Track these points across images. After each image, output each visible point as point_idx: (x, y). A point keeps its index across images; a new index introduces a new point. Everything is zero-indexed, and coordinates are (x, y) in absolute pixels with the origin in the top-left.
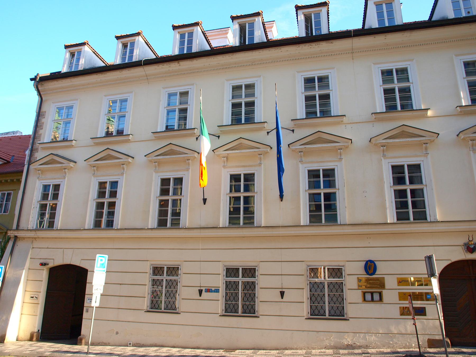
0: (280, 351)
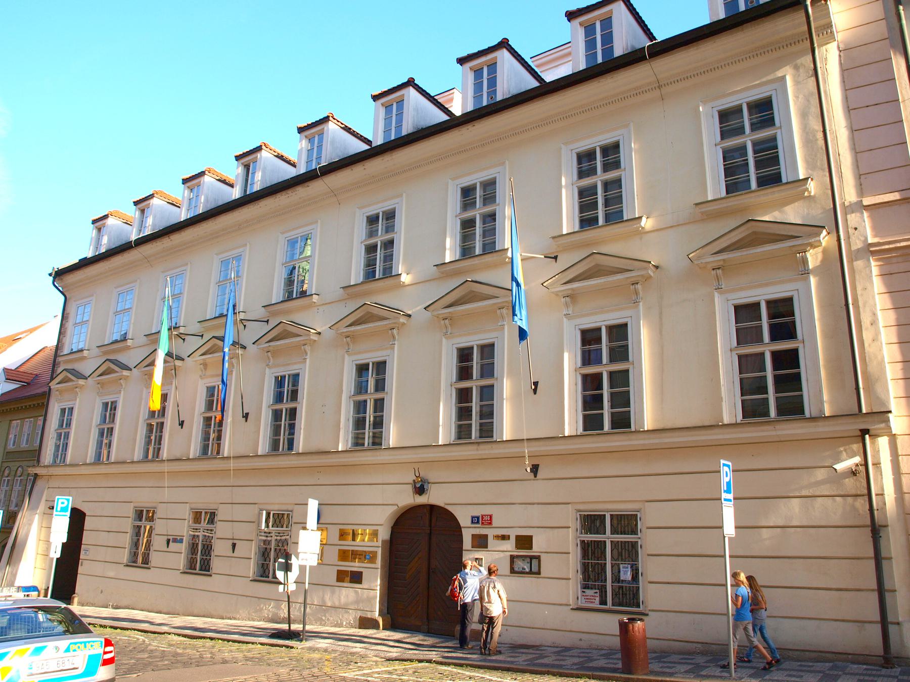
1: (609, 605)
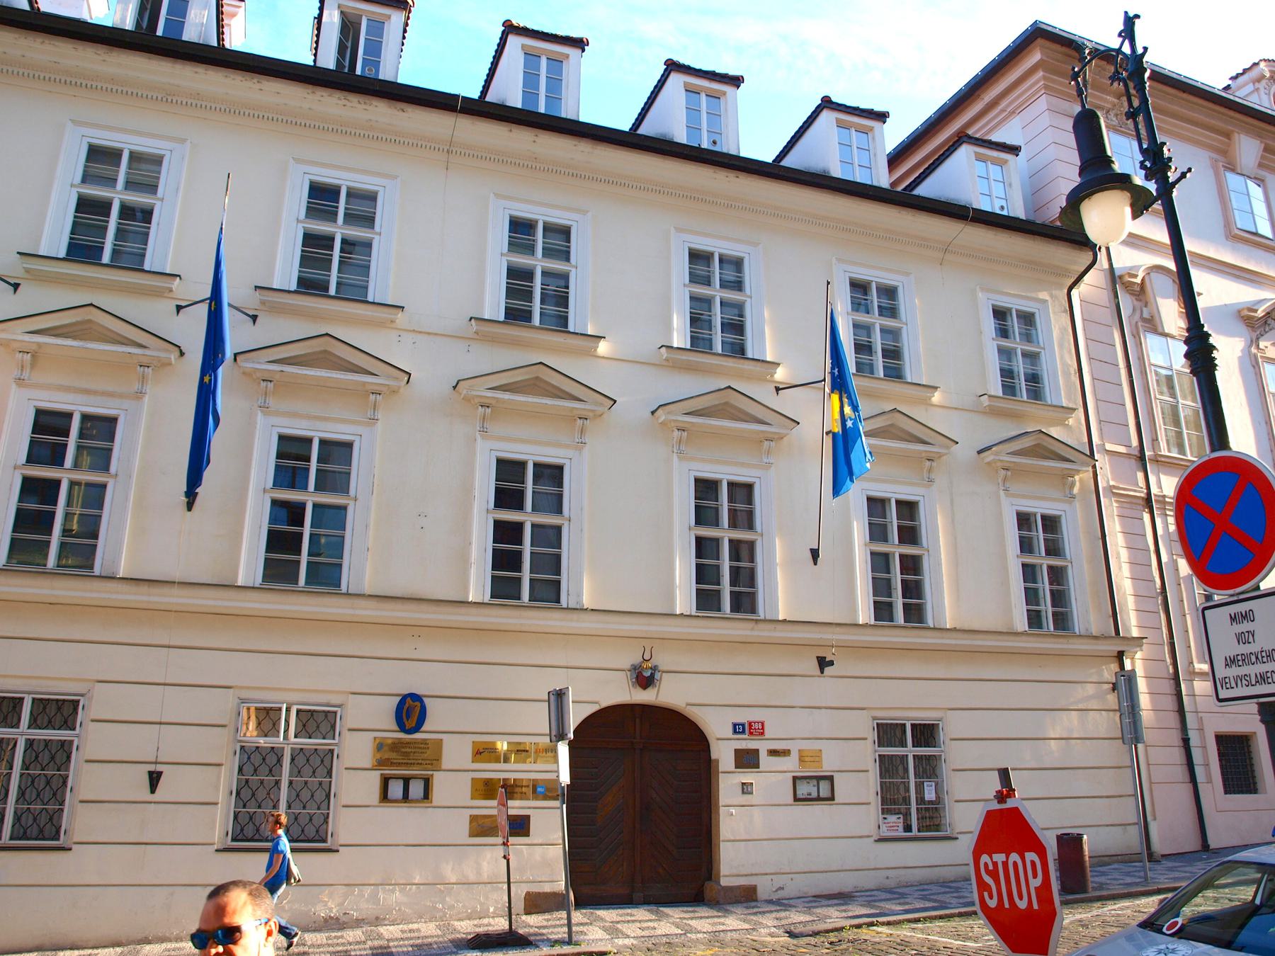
0: (125, 948)
1: (915, 832)
